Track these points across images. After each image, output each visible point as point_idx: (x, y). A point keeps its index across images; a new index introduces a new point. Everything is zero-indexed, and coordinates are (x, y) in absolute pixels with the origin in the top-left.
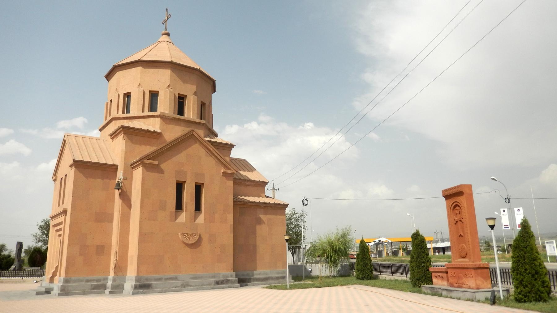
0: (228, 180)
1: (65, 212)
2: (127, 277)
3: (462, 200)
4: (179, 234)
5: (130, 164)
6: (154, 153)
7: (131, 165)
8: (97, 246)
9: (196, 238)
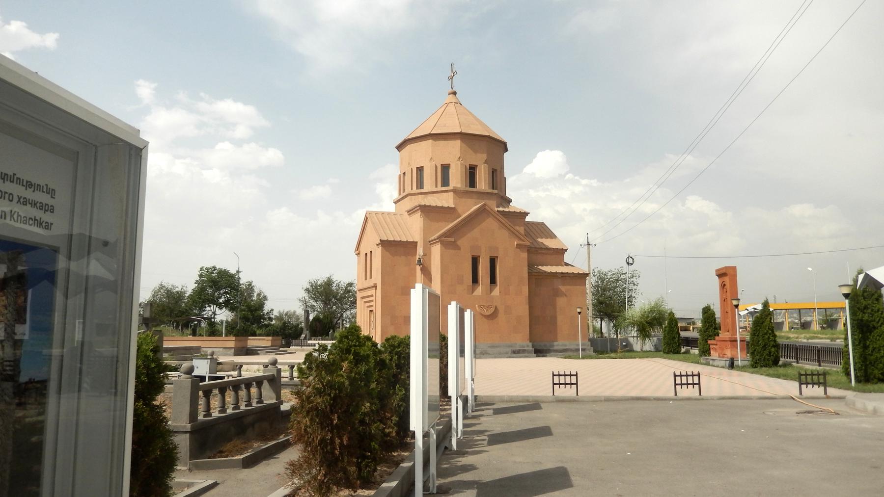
0: (522, 252)
1: (375, 286)
3: (727, 280)
4: (477, 306)
7: (429, 242)
9: (493, 310)
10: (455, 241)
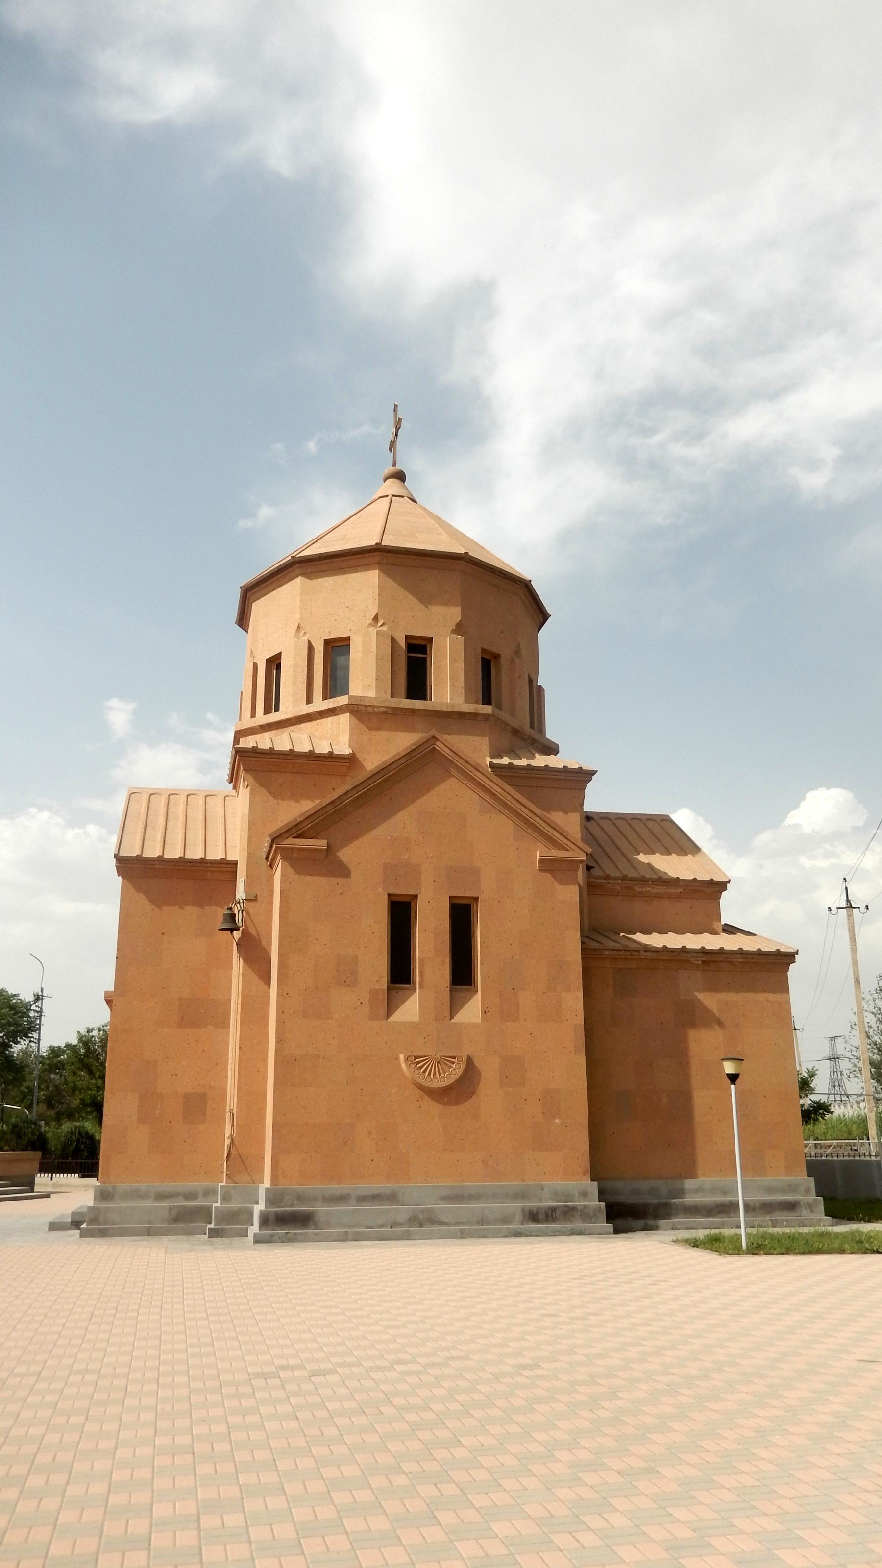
0: (560, 884)
6: (314, 818)
8: (187, 1096)
9: (456, 1071)
10: (329, 850)
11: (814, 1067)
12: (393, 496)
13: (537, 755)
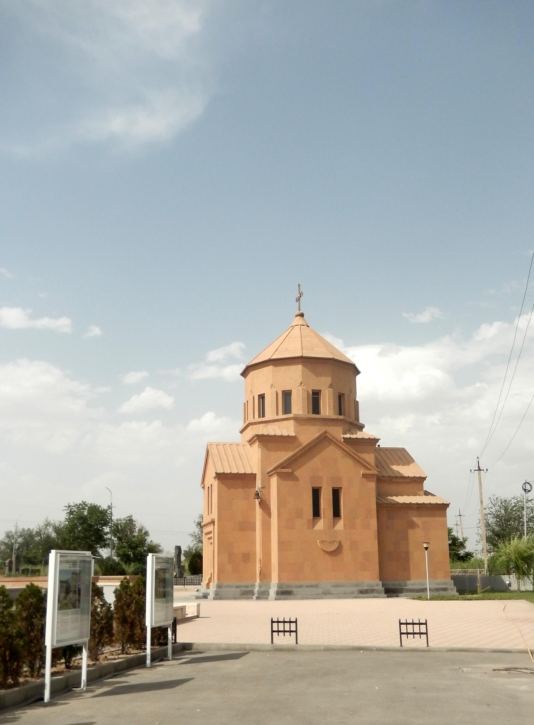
1: (213, 522)
2: (271, 583)
4: (318, 541)
5: (267, 472)
7: (268, 473)
10: (292, 473)
11: (466, 537)
12: (301, 325)
13: (358, 432)
